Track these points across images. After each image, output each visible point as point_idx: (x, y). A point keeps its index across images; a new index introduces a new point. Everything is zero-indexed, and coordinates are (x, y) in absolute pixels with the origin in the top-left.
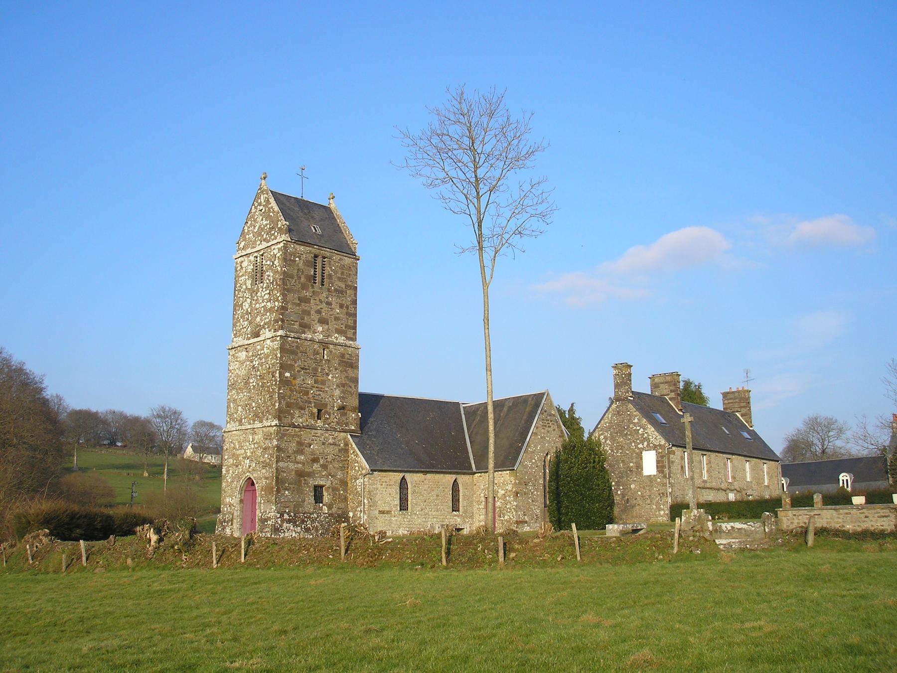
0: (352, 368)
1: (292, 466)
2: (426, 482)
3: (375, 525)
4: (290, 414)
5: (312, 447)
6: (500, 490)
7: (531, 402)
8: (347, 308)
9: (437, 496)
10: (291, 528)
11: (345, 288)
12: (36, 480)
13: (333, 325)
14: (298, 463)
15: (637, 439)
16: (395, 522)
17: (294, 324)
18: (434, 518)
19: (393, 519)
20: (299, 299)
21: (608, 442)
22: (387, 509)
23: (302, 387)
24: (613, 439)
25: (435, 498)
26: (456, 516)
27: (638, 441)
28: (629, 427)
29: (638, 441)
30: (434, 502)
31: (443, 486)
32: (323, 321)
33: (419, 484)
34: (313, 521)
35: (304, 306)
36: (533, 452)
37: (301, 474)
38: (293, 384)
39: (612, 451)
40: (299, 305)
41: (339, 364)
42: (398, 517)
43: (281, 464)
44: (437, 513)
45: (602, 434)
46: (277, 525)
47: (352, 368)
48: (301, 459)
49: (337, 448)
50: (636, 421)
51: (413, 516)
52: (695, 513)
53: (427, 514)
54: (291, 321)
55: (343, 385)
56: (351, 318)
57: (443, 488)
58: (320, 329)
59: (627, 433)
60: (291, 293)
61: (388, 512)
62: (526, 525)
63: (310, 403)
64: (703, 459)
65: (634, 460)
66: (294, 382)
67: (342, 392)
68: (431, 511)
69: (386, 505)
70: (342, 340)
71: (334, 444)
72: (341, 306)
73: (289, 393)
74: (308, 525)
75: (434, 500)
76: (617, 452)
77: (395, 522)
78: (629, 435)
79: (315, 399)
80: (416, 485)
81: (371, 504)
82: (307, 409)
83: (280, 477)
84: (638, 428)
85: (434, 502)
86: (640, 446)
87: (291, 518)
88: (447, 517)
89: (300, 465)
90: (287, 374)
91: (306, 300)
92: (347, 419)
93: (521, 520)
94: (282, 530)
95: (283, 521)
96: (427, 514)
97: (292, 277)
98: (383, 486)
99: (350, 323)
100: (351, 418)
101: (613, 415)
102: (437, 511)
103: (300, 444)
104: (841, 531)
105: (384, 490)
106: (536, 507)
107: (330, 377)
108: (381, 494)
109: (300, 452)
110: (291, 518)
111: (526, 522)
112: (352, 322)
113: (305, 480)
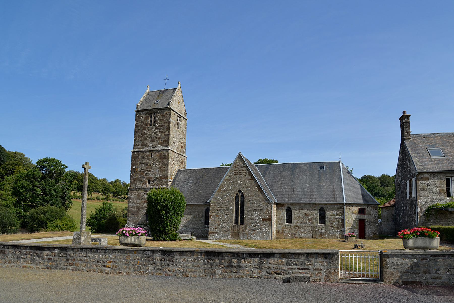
0: (165, 159)
1: (135, 205)
4: (135, 183)
5: (144, 196)
7: (238, 162)
8: (165, 132)
11: (164, 124)
12: (409, 217)
13: (157, 141)
14: (137, 203)
17: (139, 146)
18: (192, 228)
20: (142, 134)
32: (152, 141)
35: (143, 137)
36: (225, 191)
38: (137, 170)
41: (159, 158)
44: (194, 226)
47: (165, 159)
54: (138, 144)
55: (161, 168)
56: (167, 136)
57: (198, 213)
60: (138, 133)
62: (217, 234)
63: (144, 177)
64: (410, 186)
66: (137, 170)
67: (160, 171)
68: (190, 225)
70: (162, 147)
72: (162, 132)
73: (134, 174)
79: (146, 176)
82: (143, 180)
88: (200, 228)
89: (138, 205)
91: (145, 134)
92: (162, 183)
93: (212, 231)
97: (139, 126)
99: (166, 138)
100: (164, 182)
102: (194, 224)
103: (139, 195)
104: (227, 243)
106: (226, 224)
107: (154, 165)
109: (139, 199)
111: (217, 233)
112: (167, 138)
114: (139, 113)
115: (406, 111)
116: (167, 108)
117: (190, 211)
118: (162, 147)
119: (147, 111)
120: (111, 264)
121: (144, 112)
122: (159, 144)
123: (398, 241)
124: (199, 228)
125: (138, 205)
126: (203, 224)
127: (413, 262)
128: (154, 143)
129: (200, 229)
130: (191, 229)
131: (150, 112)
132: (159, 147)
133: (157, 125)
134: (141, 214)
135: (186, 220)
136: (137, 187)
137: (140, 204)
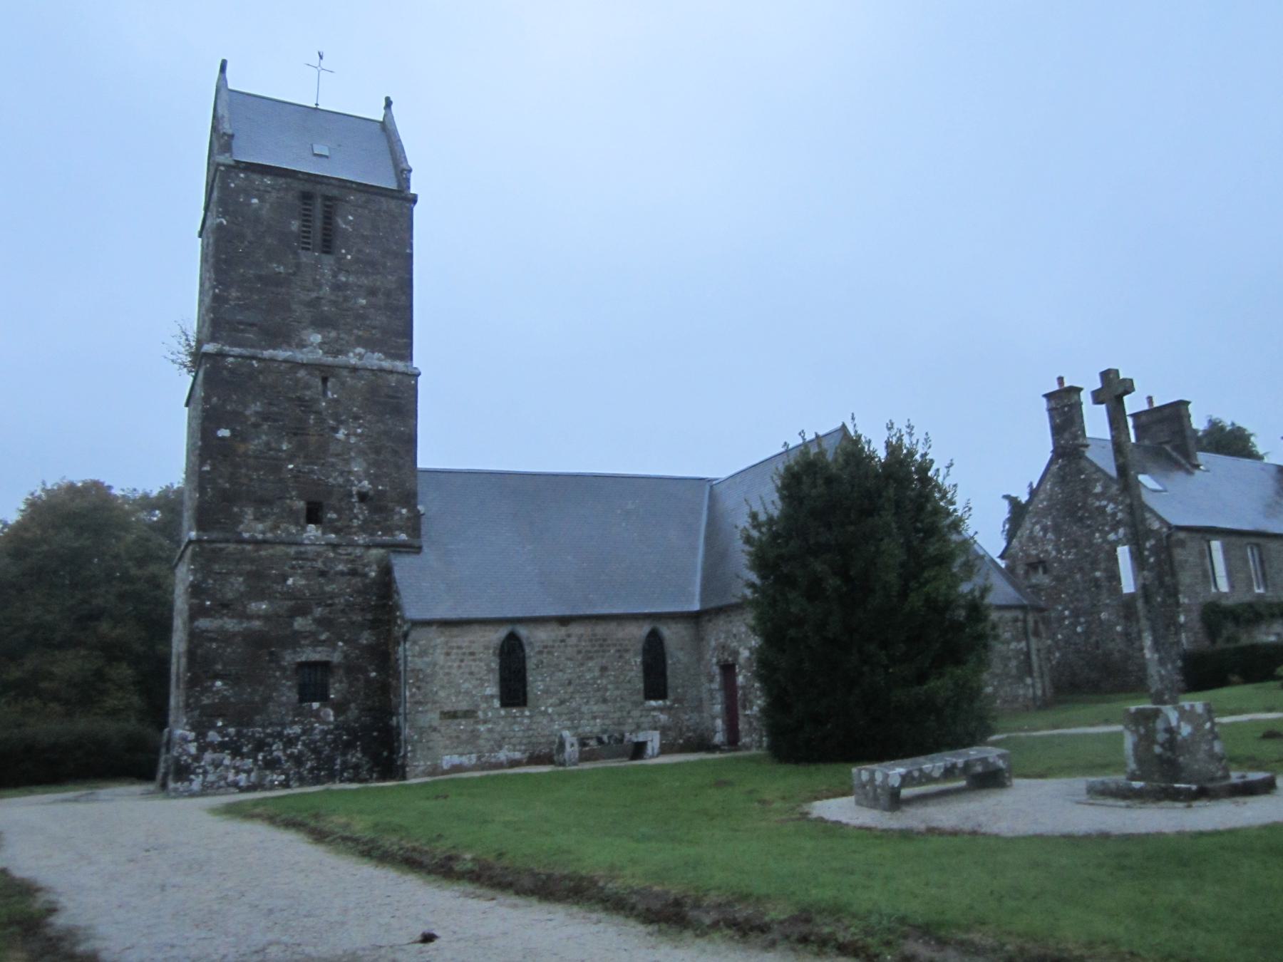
2: (573, 640)
3: (431, 744)
6: (741, 650)
9: (604, 669)
10: (227, 761)
15: (1104, 525)
16: (486, 735)
19: (482, 728)
21: (1050, 535)
22: (464, 705)
23: (265, 458)
24: (1057, 529)
25: (597, 674)
26: (654, 709)
27: (1107, 529)
28: (1085, 503)
29: (1107, 529)
30: (595, 683)
31: (619, 647)
32: (321, 323)
33: (553, 647)
34: (290, 742)
37: (257, 642)
39: (1059, 551)
42: (495, 723)
43: (203, 623)
44: (603, 707)
45: (1036, 523)
46: (185, 757)
48: (260, 609)
49: (356, 581)
50: (1098, 489)
51: (540, 719)
52: (1167, 721)
53: (578, 710)
57: (619, 651)
58: (317, 338)
59: (1083, 515)
61: (469, 714)
65: (1103, 566)
69: (460, 698)
70: (376, 360)
71: (353, 573)
74: (275, 754)
75: (594, 679)
76: (1068, 553)
77: (486, 735)
78: (1088, 518)
80: (546, 649)
81: (419, 697)
83: (199, 651)
84: (1104, 503)
85: (595, 683)
86: (1112, 537)
87: (227, 739)
90: (224, 433)
94: (199, 767)
95: (202, 749)
96: (578, 710)
98: (453, 657)
101: (1054, 485)
105: (456, 665)
108: (448, 674)
110: (227, 739)
113: (271, 653)
114: (242, 175)
115: (1187, 403)
116: (397, 194)
117: (583, 644)
118: (376, 360)
119: (289, 180)
120: (597, 929)
121: (269, 178)
122: (360, 342)
123: (178, 687)
124: (625, 714)
126: (641, 697)
127: (565, 760)
128: (333, 334)
129: (630, 721)
130: (592, 722)
131: (307, 187)
132: (361, 357)
133: (346, 254)
134: (278, 674)
135: (570, 683)
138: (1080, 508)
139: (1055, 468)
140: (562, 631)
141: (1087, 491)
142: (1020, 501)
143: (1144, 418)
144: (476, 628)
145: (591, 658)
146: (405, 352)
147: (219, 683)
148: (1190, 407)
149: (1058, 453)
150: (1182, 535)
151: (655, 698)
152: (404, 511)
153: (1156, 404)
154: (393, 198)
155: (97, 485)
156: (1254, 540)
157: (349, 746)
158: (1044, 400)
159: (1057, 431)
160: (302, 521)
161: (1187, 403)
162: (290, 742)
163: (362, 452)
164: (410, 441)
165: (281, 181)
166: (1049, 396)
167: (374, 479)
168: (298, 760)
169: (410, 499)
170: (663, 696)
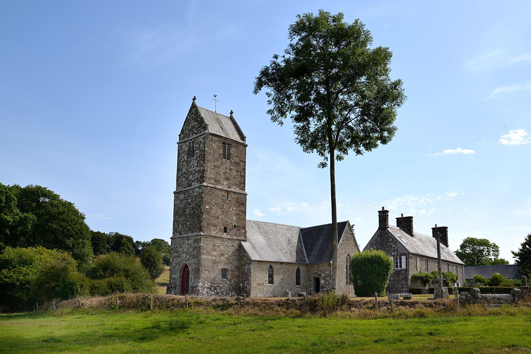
17: (211, 180)
22: (262, 282)
26: (298, 287)
29: (392, 251)
32: (227, 179)
40: (214, 169)
50: (391, 240)
58: (226, 183)
75: (287, 278)
78: (387, 248)
84: (392, 244)
115: (447, 228)
118: (237, 190)
122: (235, 184)
125: (214, 258)
126: (295, 284)
131: (224, 141)
136: (212, 234)
137: (216, 256)
138: (385, 245)
139: (378, 232)
140: (281, 266)
141: (387, 241)
142: (524, 243)
143: (400, 220)
144: (264, 263)
145: (286, 273)
146: (244, 189)
147: (206, 272)
148: (448, 229)
149: (380, 228)
150: (411, 255)
151: (298, 285)
152: (243, 231)
153: (404, 216)
154: (242, 145)
155: (488, 241)
156: (427, 259)
157: (232, 290)
158: (378, 213)
159: (380, 222)
160: (223, 232)
161: (447, 228)
162: (221, 288)
163: (235, 215)
164: (245, 212)
165: (219, 139)
166: (379, 212)
167: (237, 222)
168: (222, 292)
169: (244, 228)
170: (299, 285)
